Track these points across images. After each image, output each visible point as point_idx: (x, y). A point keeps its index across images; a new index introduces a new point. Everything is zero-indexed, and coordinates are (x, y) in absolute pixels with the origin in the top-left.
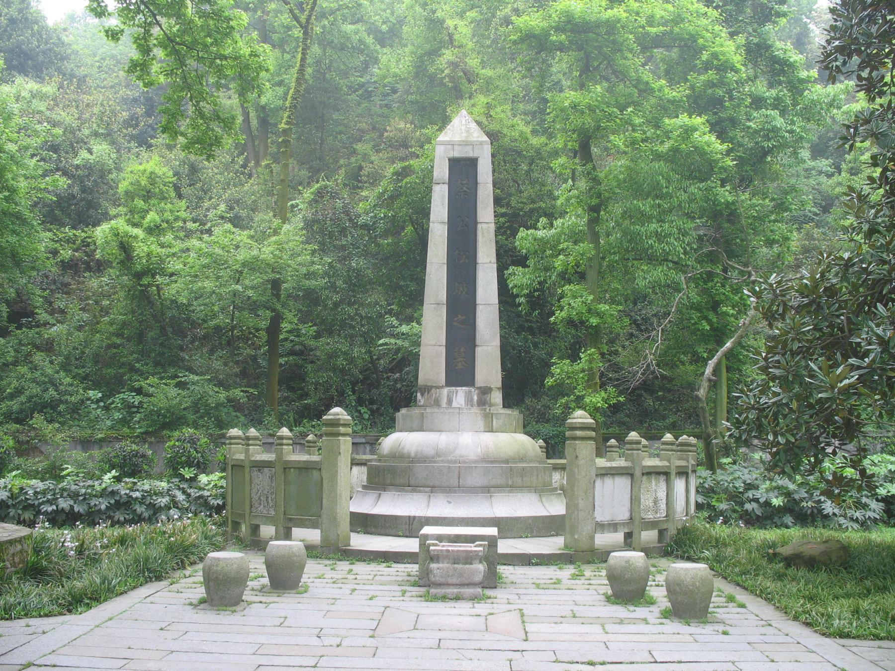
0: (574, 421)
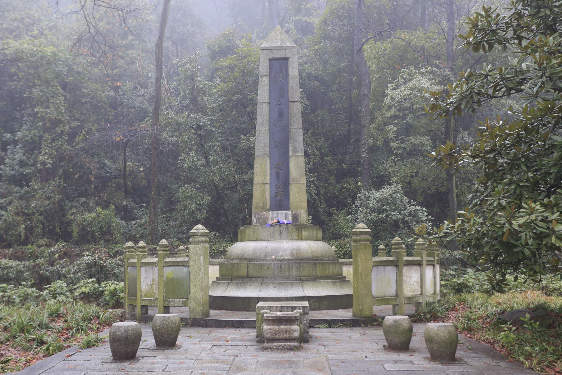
0: (357, 230)
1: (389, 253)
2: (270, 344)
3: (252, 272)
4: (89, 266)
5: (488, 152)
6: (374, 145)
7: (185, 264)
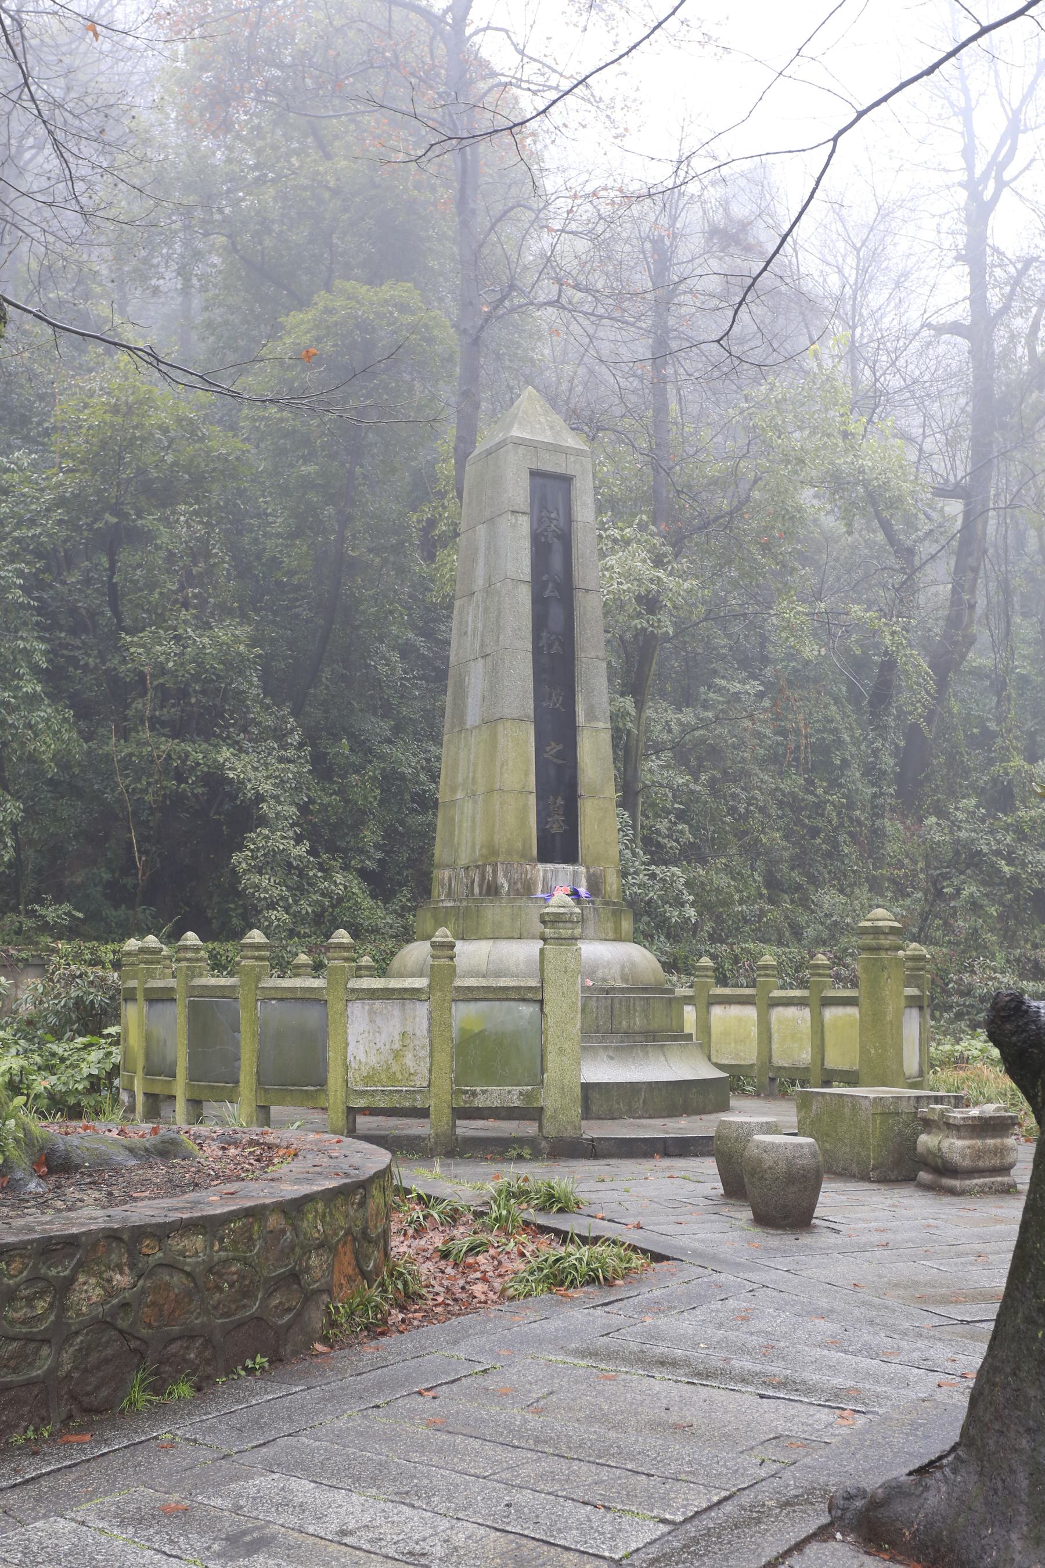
2: (968, 1182)
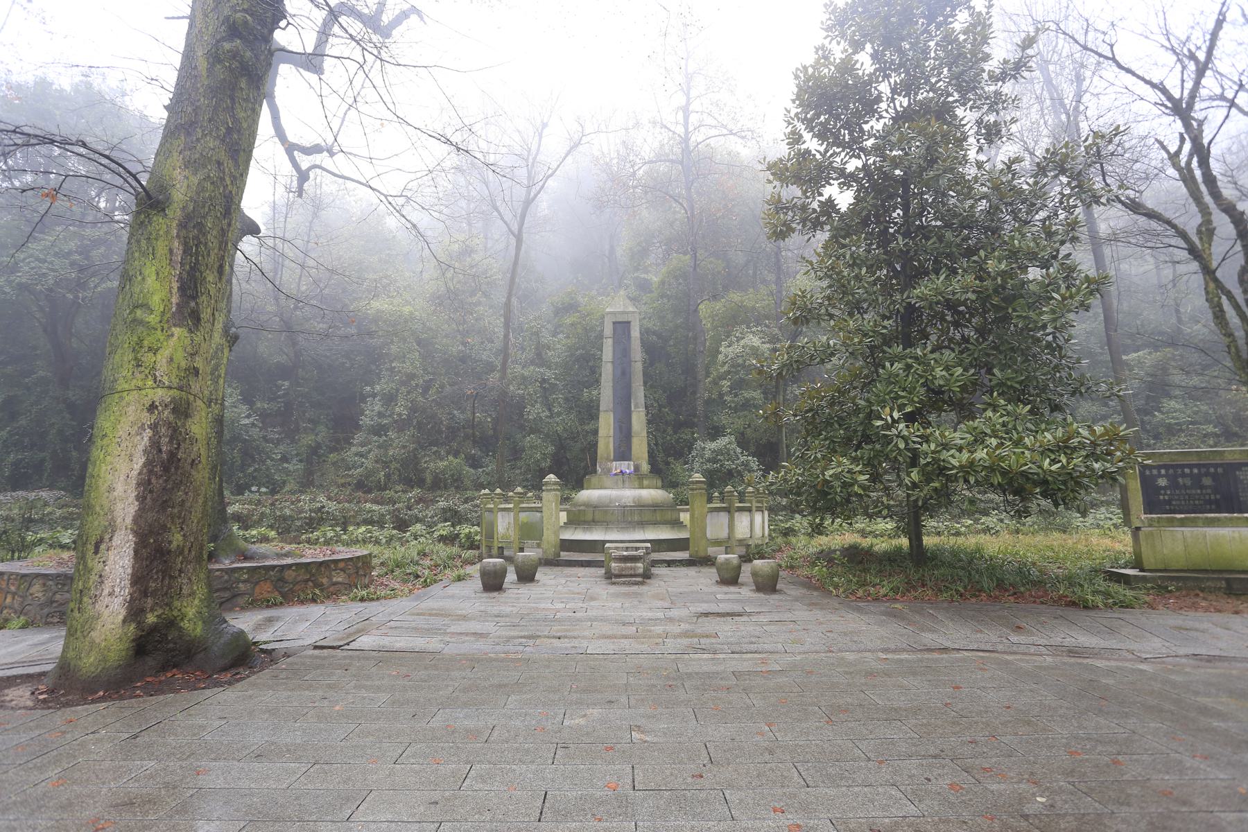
1: (722, 501)
3: (597, 518)
4: (444, 510)
5: (807, 412)
6: (710, 398)
7: (539, 510)
